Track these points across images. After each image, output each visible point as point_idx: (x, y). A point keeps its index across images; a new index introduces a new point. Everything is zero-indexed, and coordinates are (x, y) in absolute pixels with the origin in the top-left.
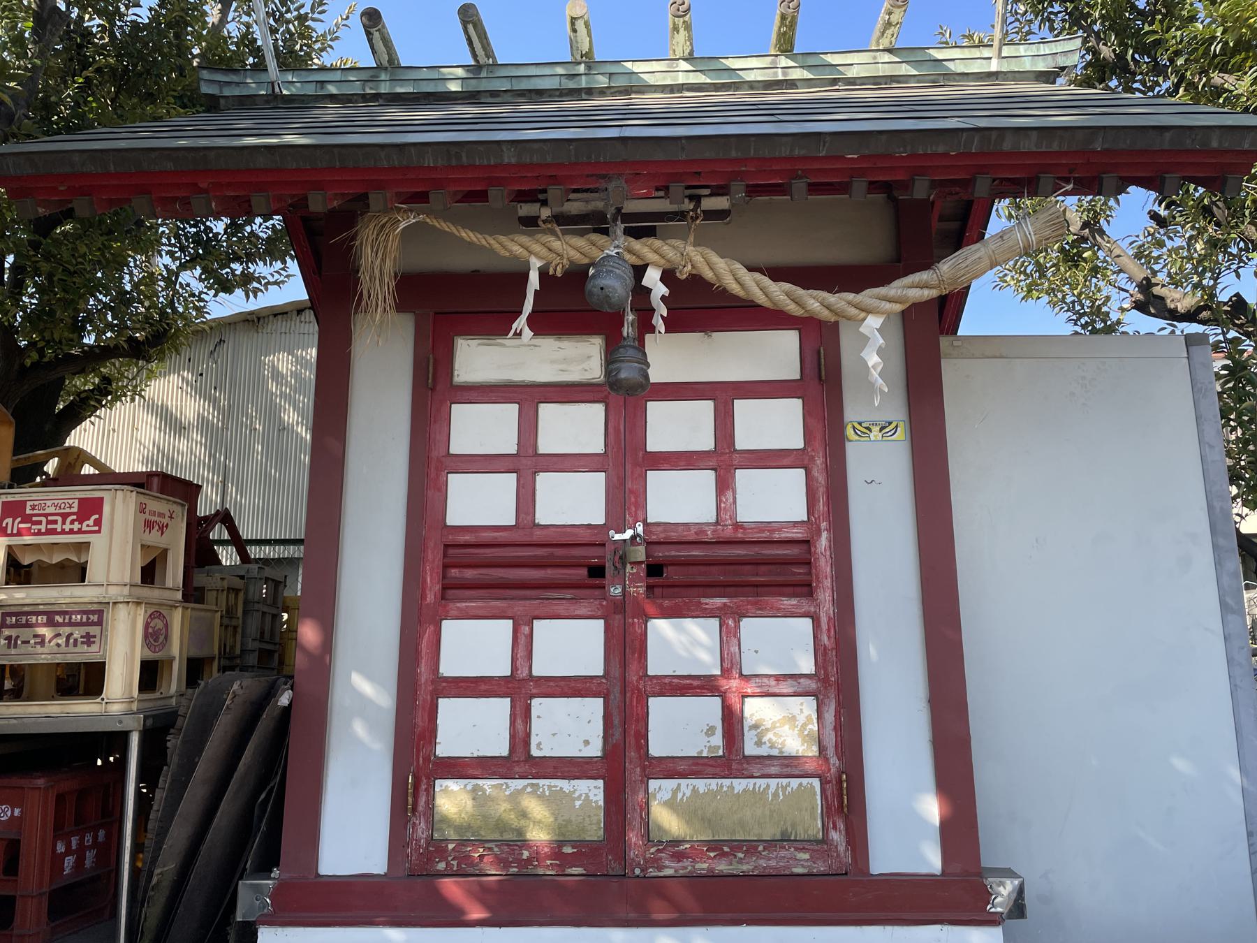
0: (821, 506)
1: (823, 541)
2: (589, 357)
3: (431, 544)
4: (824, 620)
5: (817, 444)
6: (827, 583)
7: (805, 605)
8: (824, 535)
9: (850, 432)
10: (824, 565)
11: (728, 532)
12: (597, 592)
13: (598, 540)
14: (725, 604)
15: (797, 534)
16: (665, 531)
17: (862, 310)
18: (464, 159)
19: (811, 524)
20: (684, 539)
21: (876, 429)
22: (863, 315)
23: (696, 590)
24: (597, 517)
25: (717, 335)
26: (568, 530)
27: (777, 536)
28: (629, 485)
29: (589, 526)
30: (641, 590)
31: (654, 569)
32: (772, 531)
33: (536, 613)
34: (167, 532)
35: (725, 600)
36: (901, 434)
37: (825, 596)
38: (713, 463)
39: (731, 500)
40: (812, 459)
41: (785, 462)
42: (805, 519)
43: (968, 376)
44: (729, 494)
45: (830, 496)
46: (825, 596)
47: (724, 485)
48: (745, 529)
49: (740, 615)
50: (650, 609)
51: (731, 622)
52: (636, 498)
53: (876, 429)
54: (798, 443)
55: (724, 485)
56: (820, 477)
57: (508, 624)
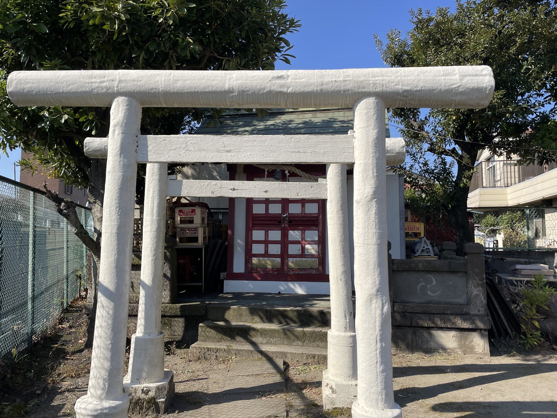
10: (321, 222)
15: (316, 215)
19: (318, 214)
31: (290, 222)
37: (320, 227)
46: (320, 227)
47: (303, 206)
55: (303, 206)
56: (250, 239)
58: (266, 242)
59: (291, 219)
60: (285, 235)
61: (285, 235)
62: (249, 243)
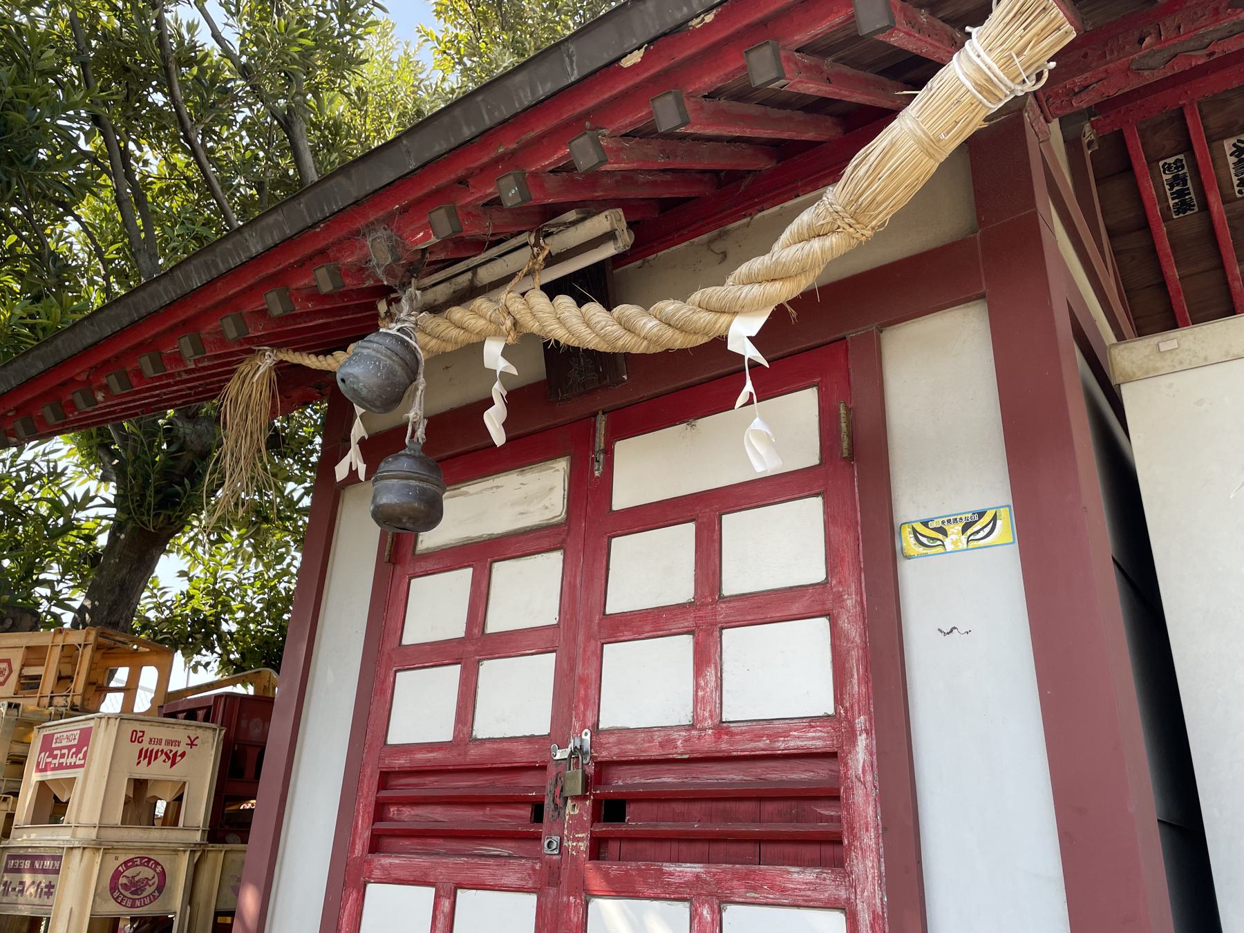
0: (855, 686)
1: (861, 754)
2: (551, 489)
3: (368, 771)
4: (865, 918)
5: (847, 571)
6: (869, 839)
7: (831, 886)
8: (862, 741)
9: (907, 541)
10: (864, 803)
11: (707, 743)
12: (528, 846)
13: (538, 760)
14: (697, 876)
15: (815, 740)
16: (619, 743)
17: (722, 312)
18: (221, 265)
19: (840, 722)
20: (644, 756)
21: (954, 530)
22: (724, 319)
23: (649, 848)
24: (542, 726)
25: (702, 422)
26: (505, 745)
27: (781, 746)
28: (579, 670)
29: (531, 739)
30: (583, 846)
31: (611, 809)
32: (774, 737)
33: (459, 878)
34: (181, 763)
35: (698, 868)
36: (1005, 531)
37: (867, 863)
38: (689, 623)
39: (712, 684)
40: (839, 598)
41: (795, 609)
42: (831, 711)
43: (1200, 402)
44: (710, 674)
45: (876, 667)
46: (867, 863)
47: (706, 658)
48: (732, 734)
49: (722, 900)
50: (595, 882)
51: (706, 912)
52: (586, 689)
53: (954, 530)
54: (814, 572)
55: (706, 658)
56: (853, 630)
57: (430, 892)
58: (707, 616)
59: (623, 781)
60: (576, 691)
61: (576, 691)
62: (864, 597)
